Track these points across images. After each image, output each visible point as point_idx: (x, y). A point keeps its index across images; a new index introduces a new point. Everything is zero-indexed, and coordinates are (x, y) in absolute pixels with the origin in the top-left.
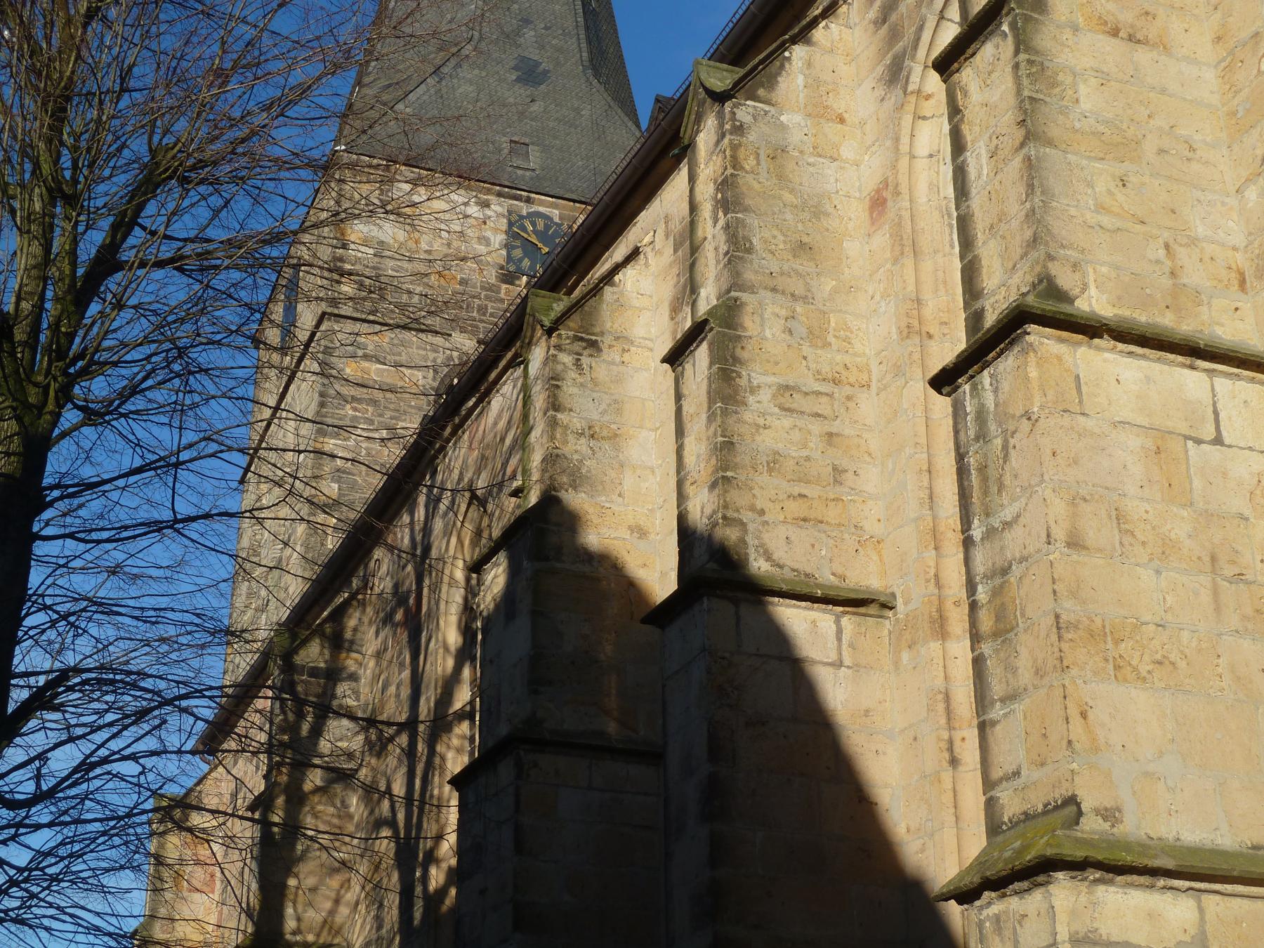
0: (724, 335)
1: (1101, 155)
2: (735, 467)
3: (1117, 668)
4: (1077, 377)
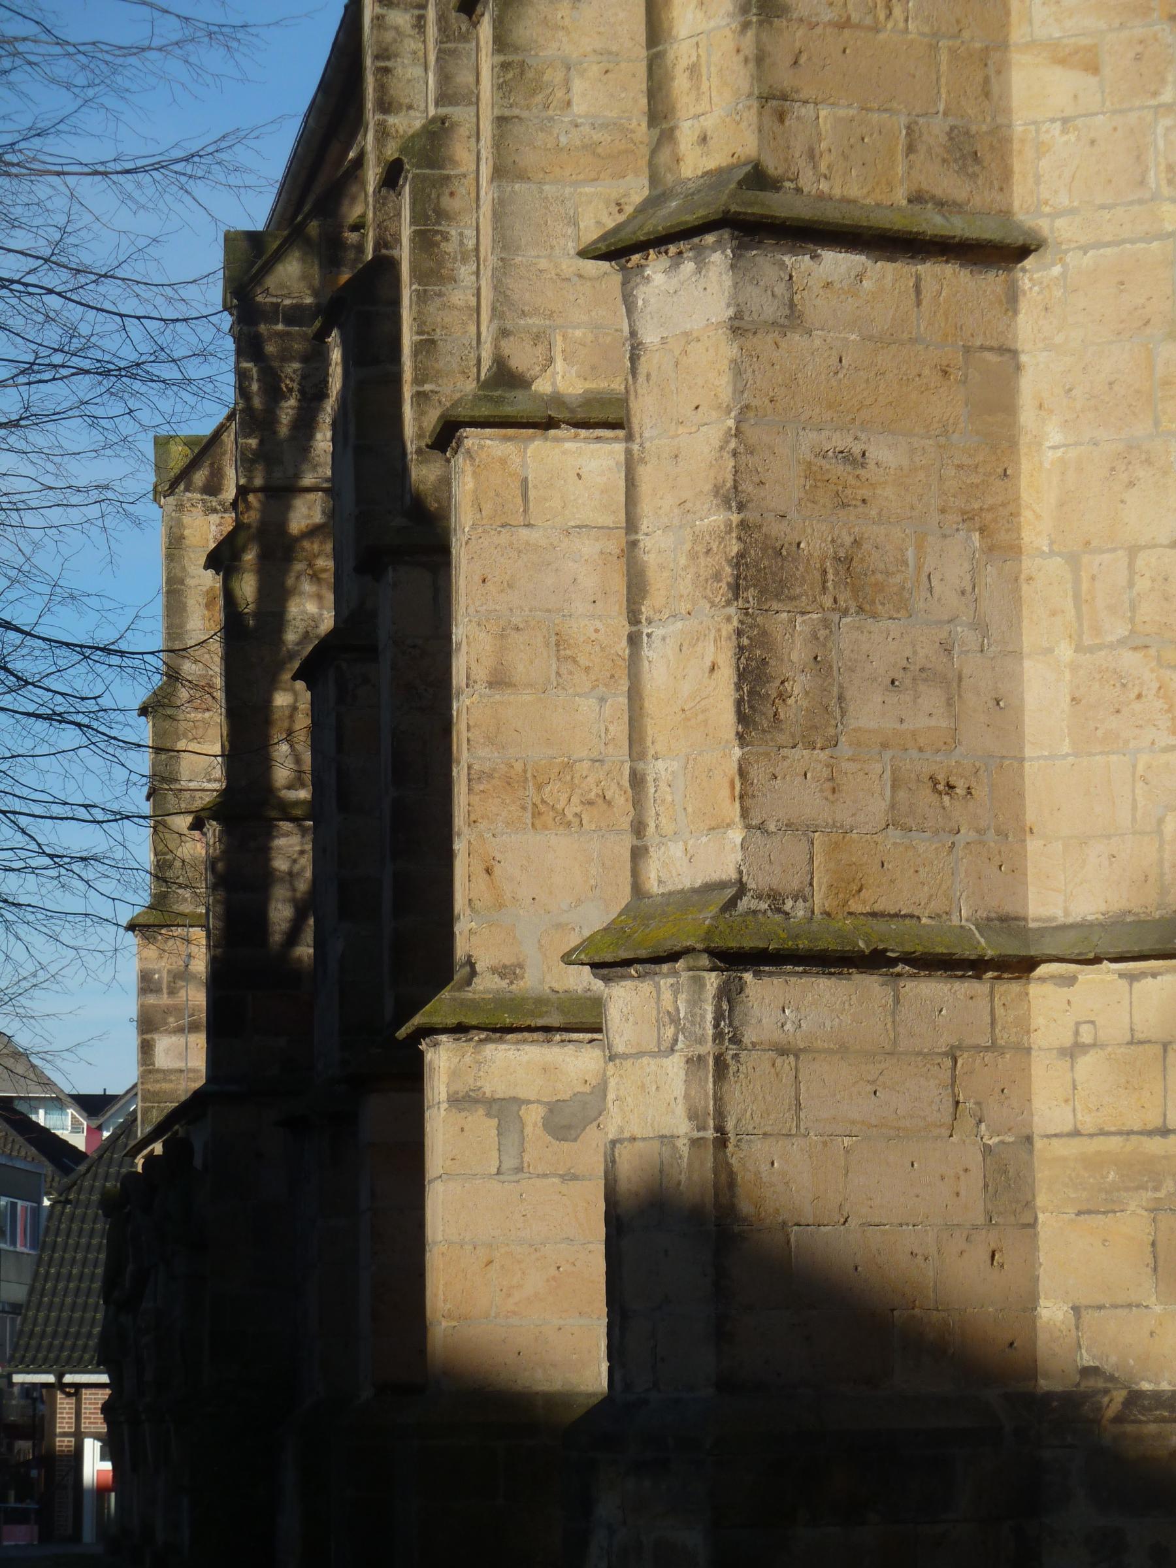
0: (425, 178)
1: (593, 175)
2: (438, 374)
3: (537, 814)
4: (525, 480)
